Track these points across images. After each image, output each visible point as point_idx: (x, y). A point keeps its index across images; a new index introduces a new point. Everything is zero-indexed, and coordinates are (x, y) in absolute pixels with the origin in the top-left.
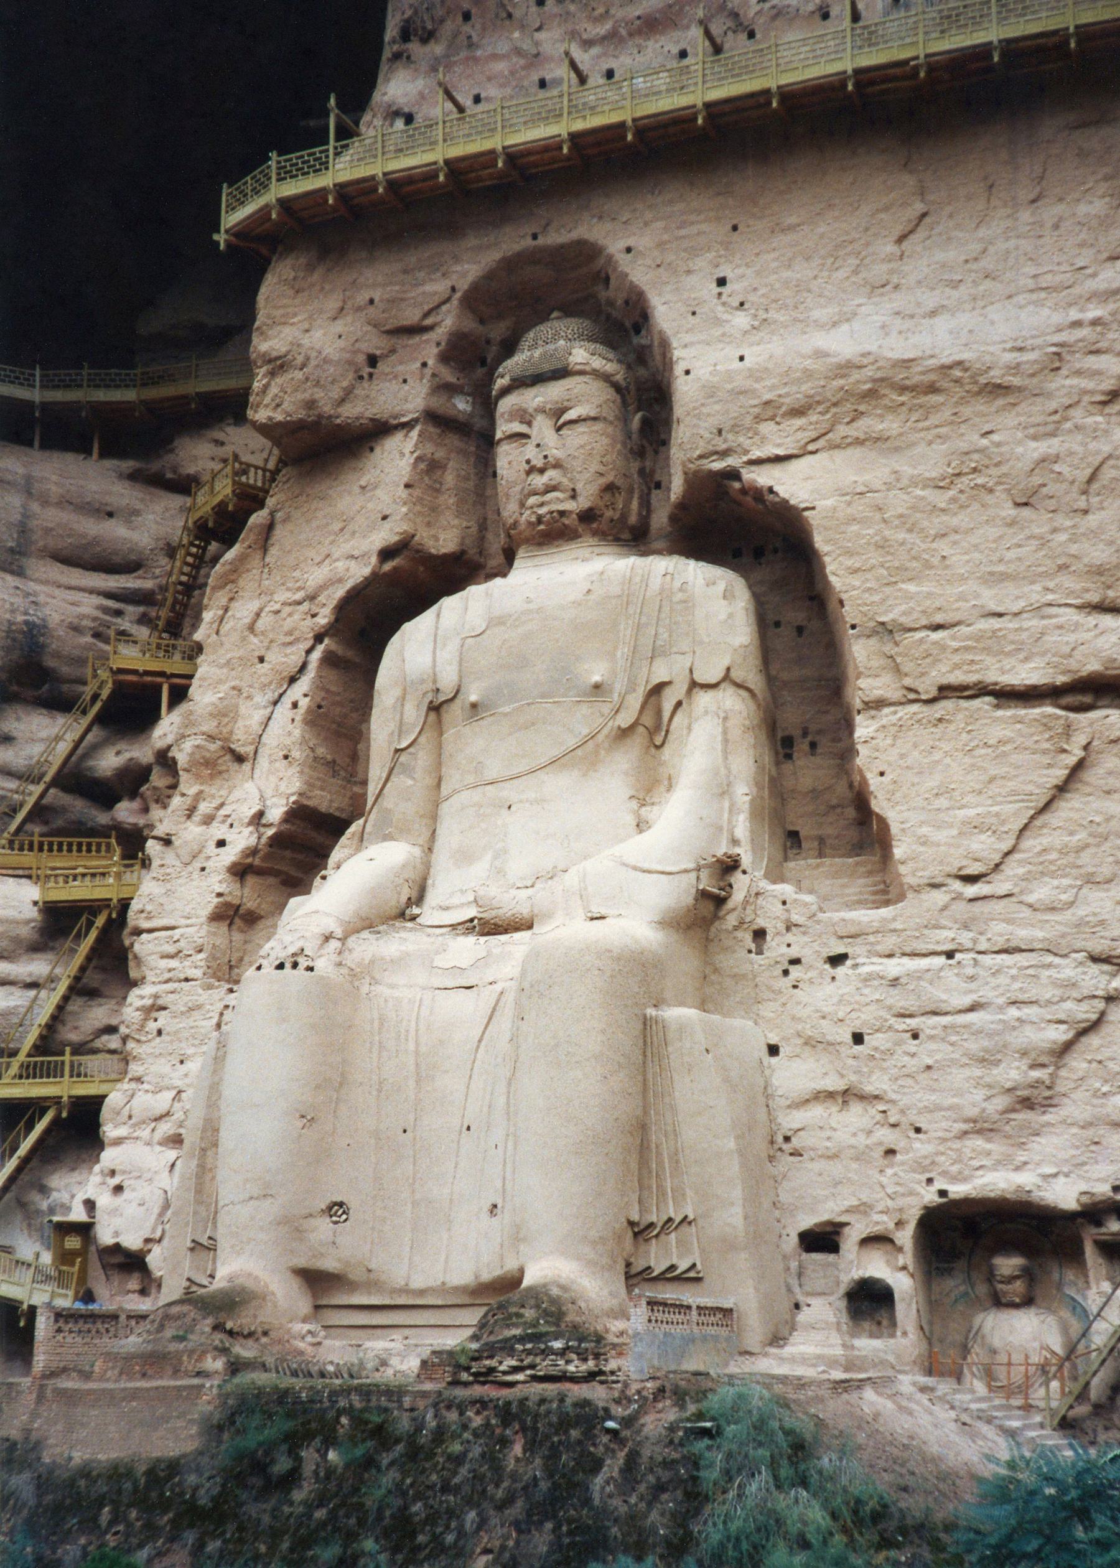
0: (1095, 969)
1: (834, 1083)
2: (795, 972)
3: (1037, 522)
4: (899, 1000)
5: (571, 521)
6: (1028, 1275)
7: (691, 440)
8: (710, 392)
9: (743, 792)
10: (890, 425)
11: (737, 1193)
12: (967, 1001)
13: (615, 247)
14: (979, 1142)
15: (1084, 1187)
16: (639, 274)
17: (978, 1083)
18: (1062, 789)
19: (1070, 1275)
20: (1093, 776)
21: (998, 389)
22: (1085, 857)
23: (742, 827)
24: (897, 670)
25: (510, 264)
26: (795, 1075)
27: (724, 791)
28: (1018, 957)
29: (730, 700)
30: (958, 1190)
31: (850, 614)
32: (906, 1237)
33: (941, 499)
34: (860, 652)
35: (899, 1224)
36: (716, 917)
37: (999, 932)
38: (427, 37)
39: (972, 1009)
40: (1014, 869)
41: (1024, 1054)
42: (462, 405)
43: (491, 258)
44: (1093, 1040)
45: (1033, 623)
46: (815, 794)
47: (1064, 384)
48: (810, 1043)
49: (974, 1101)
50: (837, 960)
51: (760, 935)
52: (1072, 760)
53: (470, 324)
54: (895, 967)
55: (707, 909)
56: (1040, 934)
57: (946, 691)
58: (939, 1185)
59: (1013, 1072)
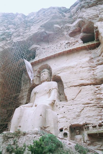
0: (83, 105)
1: (63, 116)
2: (60, 108)
3: (76, 75)
4: (67, 109)
5: (45, 80)
6: (80, 132)
7: (53, 73)
8: (54, 70)
9: (56, 96)
10: (66, 70)
11: (53, 124)
12: (73, 108)
13: (48, 64)
14: (74, 120)
15: (83, 122)
16: (50, 65)
17: (74, 115)
18: (79, 92)
19: (83, 131)
20: (81, 91)
21: (73, 67)
22: (81, 97)
23: (56, 98)
24: (67, 86)
25: (42, 66)
26: (60, 116)
27: (55, 96)
28: (77, 105)
29: (55, 90)
30: (73, 124)
31: (63, 82)
32: (68, 128)
33: (70, 74)
34: (64, 85)
35: (68, 127)
36: (54, 105)
37: (75, 103)
38: (38, 55)
39: (73, 109)
40: (76, 98)
41: (77, 112)
42: (39, 75)
43: (41, 66)
44: (83, 111)
45: (77, 81)
46: (62, 98)
47: (77, 67)
48: (61, 113)
49: (74, 116)
50: (63, 107)
51: (57, 106)
52: (80, 90)
53: (39, 70)
54: (67, 107)
55: (53, 104)
56: (78, 103)
57: (70, 86)
58: (71, 124)
59: (77, 113)
